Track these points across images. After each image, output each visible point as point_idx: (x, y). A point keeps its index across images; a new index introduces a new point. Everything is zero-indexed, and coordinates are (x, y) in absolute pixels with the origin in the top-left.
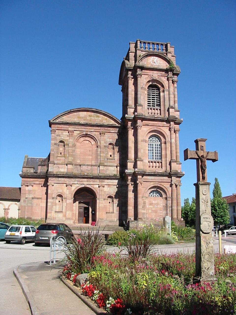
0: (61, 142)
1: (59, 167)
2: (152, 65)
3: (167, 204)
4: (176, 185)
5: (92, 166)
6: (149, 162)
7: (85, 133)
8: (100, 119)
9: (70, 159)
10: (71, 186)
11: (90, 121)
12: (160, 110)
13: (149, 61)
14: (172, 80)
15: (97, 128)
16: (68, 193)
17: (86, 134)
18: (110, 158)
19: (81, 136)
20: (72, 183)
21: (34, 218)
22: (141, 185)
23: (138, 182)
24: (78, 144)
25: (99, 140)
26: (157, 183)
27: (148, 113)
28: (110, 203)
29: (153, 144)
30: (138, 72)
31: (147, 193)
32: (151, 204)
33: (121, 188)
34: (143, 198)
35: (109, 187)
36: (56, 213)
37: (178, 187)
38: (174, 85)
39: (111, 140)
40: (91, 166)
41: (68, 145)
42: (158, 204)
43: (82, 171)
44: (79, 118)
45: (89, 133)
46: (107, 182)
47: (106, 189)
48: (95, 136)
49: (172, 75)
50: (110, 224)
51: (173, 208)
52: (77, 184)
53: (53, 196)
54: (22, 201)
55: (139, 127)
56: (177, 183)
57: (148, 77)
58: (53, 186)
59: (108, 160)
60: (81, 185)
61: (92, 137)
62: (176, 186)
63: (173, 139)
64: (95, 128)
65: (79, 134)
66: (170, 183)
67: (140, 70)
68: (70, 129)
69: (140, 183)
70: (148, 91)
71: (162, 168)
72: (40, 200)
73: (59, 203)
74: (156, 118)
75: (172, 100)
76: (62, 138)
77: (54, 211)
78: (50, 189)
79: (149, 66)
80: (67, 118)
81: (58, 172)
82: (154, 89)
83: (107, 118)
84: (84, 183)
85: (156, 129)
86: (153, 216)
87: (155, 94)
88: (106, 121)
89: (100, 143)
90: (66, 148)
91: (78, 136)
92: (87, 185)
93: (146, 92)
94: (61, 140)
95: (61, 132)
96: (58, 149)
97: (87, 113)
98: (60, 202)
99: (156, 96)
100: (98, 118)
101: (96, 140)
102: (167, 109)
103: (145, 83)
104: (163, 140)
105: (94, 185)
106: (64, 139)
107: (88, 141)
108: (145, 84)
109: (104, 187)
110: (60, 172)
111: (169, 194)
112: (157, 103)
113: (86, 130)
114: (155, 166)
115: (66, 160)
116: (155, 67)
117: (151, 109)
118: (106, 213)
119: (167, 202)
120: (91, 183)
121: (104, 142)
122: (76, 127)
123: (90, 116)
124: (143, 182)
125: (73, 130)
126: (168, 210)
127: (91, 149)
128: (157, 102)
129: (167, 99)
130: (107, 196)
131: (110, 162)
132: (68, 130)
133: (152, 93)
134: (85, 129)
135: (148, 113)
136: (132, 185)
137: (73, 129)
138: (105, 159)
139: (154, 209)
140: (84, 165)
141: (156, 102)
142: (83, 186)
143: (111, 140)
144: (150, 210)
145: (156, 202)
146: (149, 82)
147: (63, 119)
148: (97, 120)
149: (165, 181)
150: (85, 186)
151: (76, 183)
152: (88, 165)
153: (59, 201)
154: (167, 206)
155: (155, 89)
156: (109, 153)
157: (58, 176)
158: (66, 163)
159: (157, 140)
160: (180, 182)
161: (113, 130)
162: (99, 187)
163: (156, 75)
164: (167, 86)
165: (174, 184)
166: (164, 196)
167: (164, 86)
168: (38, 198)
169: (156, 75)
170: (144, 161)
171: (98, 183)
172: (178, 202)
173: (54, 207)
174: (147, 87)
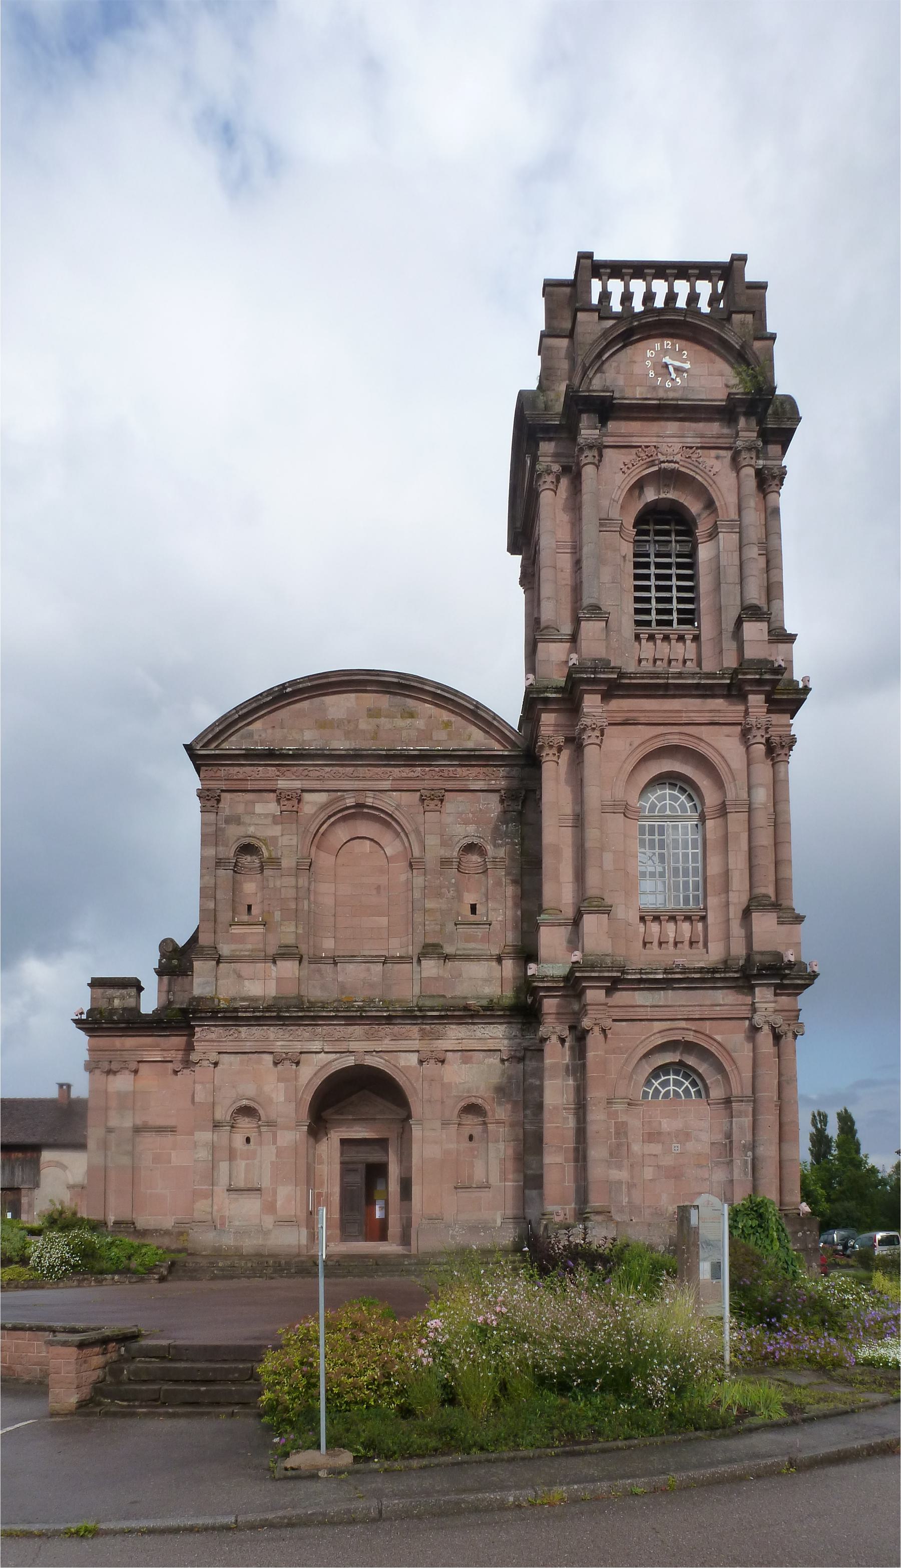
0: (248, 849)
1: (243, 974)
2: (655, 388)
3: (729, 1136)
4: (773, 1029)
6: (642, 919)
7: (350, 802)
9: (288, 933)
10: (298, 1063)
11: (375, 736)
12: (696, 638)
13: (637, 369)
14: (768, 740)
15: (406, 772)
16: (282, 1099)
17: (359, 806)
18: (472, 918)
19: (332, 819)
20: (298, 1046)
21: (143, 1222)
22: (606, 1036)
23: (586, 1023)
24: (325, 860)
25: (417, 831)
26: (683, 1024)
27: (640, 661)
28: (471, 1138)
29: (662, 828)
30: (583, 432)
31: (631, 1078)
33: (521, 1066)
34: (615, 1107)
35: (465, 1062)
36: (234, 1195)
37: (788, 1039)
38: (773, 765)
40: (384, 963)
41: (275, 862)
42: (685, 1135)
43: (342, 988)
44: (324, 724)
45: (369, 801)
46: (455, 1035)
48: (397, 815)
49: (755, 434)
51: (761, 1150)
52: (324, 1054)
53: (218, 1116)
54: (91, 1144)
55: (589, 733)
56: (779, 1020)
57: (635, 456)
58: (216, 1064)
59: (462, 929)
60: (338, 1055)
61: (384, 819)
62: (777, 1037)
63: (761, 785)
66: (747, 1022)
67: (595, 418)
68: (282, 784)
69: (597, 1029)
70: (635, 541)
71: (706, 945)
72: (169, 1138)
73: (247, 1147)
75: (754, 573)
76: (251, 830)
77: (226, 1188)
78: (202, 1083)
79: (637, 393)
80: (270, 731)
81: (234, 999)
82: (667, 533)
83: (453, 718)
84: (353, 1046)
85: (675, 740)
87: (669, 556)
88: (449, 734)
90: (267, 880)
91: (323, 816)
92: (366, 1057)
93: (627, 549)
94: (247, 841)
95: (247, 803)
96: (235, 888)
97: (357, 698)
98: (252, 1143)
100: (409, 721)
101: (402, 834)
103: (620, 494)
104: (711, 798)
105: (397, 1053)
106: (258, 834)
107: (368, 842)
108: (621, 501)
109: (443, 1062)
110: (243, 999)
111: (740, 1083)
113: (350, 782)
114: (671, 940)
116: (671, 395)
117: (651, 638)
118: (456, 1188)
119: (731, 1122)
120: (387, 1044)
121: (439, 841)
122: (311, 774)
123: (373, 713)
124: (614, 1020)
125: (299, 786)
126: (738, 1163)
129: (731, 573)
130: (459, 1107)
131: (469, 939)
132: (274, 791)
133: (657, 556)
134: (351, 778)
135: (640, 661)
136: (563, 1041)
137: (297, 784)
138: (443, 925)
139: (668, 1161)
140: (351, 958)
141: (675, 601)
142: (350, 1061)
143: (471, 829)
144: (651, 1169)
146: (639, 486)
147: (250, 735)
148: (404, 733)
149: (718, 1012)
150: (357, 1063)
151: (316, 1046)
152: (370, 960)
153: (248, 1140)
154: (731, 1142)
155: (673, 527)
156: (466, 894)
157: (232, 1016)
158: (272, 950)
159: (682, 806)
160: (798, 1016)
161: (481, 777)
162: (421, 1062)
164: (731, 499)
165: (766, 1029)
166: (716, 1093)
167: (717, 504)
168: (160, 1130)
169: (670, 441)
170: (620, 912)
171: (416, 1045)
172: (786, 1119)
173: (224, 1166)
174: (629, 521)
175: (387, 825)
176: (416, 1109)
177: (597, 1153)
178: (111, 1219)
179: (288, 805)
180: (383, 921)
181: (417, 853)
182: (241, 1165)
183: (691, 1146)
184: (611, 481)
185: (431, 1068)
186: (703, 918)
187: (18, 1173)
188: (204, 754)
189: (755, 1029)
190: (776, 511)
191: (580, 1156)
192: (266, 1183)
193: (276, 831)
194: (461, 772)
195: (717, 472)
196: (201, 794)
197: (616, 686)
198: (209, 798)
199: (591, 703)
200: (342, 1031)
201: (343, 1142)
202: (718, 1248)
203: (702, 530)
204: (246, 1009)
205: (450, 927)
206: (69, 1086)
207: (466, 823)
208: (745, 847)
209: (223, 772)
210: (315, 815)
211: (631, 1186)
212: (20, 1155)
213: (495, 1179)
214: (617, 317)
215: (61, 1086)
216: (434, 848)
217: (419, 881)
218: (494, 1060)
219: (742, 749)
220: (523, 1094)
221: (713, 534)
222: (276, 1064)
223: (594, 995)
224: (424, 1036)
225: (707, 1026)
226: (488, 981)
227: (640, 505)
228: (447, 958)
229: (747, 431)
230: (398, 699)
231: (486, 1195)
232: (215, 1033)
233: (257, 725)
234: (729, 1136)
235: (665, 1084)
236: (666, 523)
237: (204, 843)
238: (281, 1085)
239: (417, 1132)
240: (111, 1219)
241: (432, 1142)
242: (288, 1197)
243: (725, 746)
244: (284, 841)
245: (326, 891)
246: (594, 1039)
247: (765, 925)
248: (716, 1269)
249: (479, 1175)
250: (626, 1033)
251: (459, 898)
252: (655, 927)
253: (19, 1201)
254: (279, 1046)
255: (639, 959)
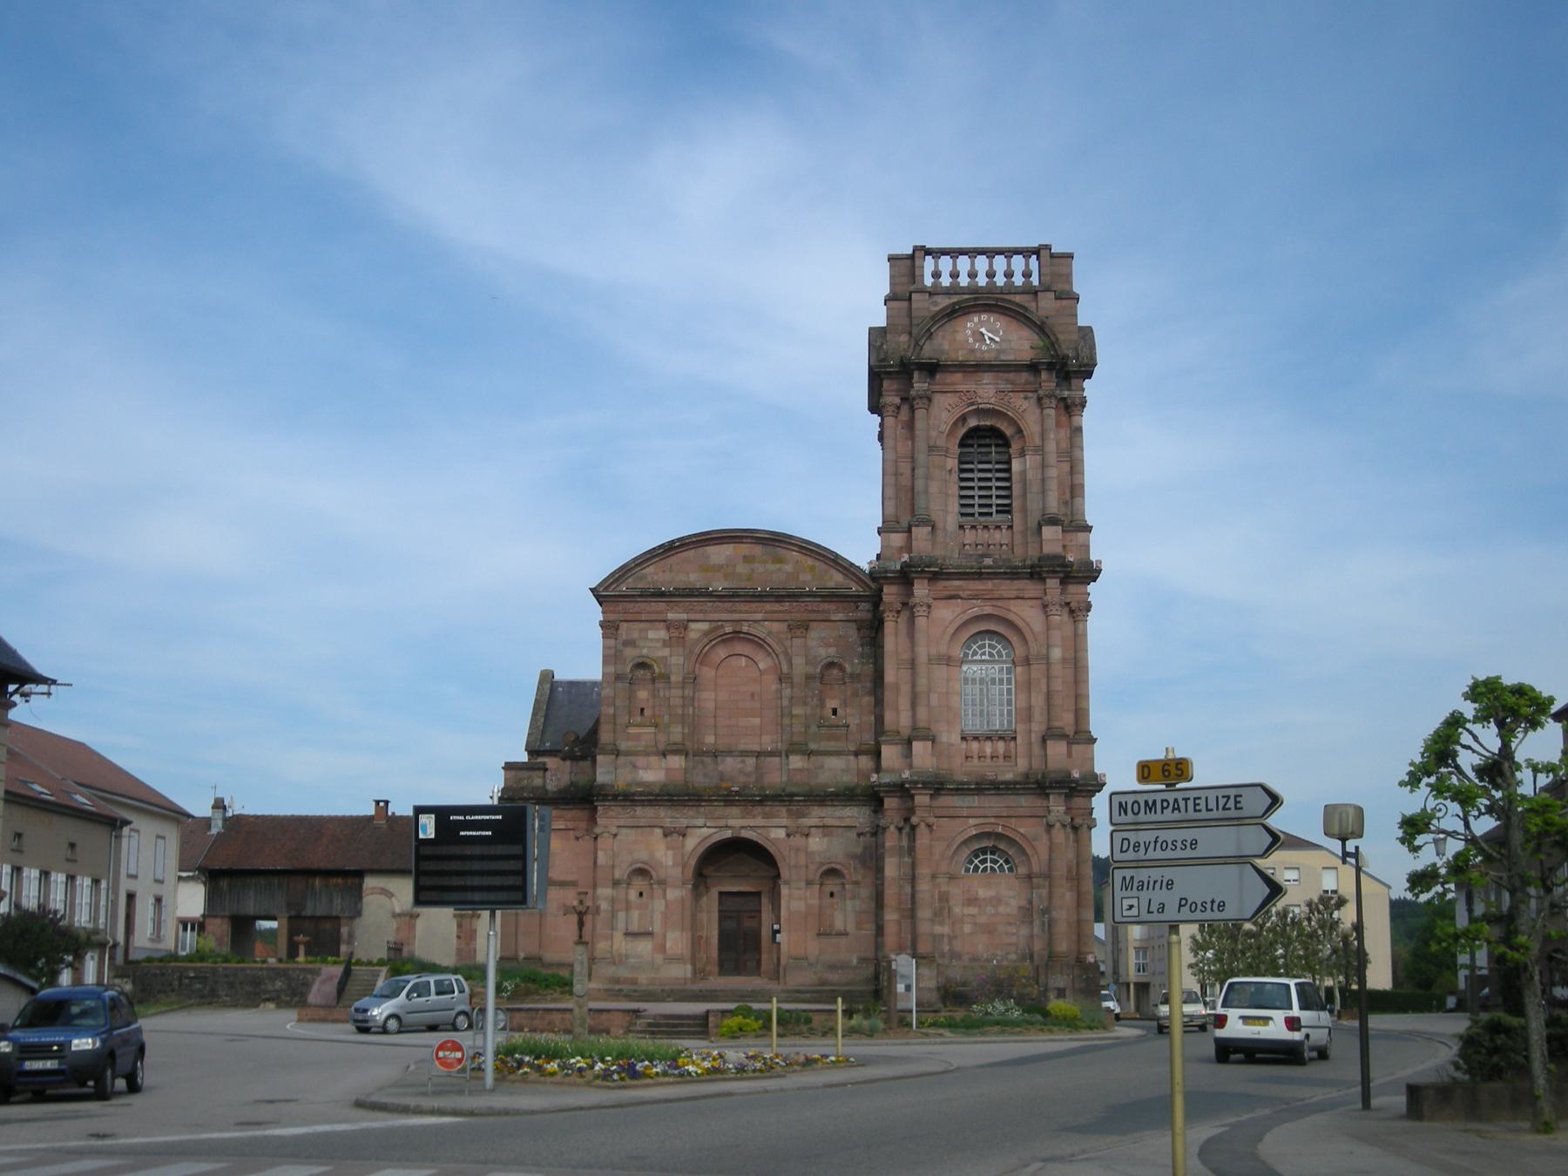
0: (642, 665)
2: (973, 351)
3: (1030, 902)
5: (759, 754)
6: (964, 738)
7: (728, 629)
8: (789, 568)
9: (677, 733)
11: (749, 578)
12: (1010, 527)
13: (959, 337)
15: (777, 607)
16: (670, 863)
20: (684, 822)
23: (914, 820)
24: (707, 673)
25: (786, 653)
28: (832, 895)
32: (972, 901)
39: (832, 651)
41: (666, 677)
42: (997, 901)
43: (722, 777)
44: (706, 568)
45: (745, 629)
46: (816, 815)
47: (816, 843)
48: (769, 640)
50: (834, 977)
52: (704, 830)
53: (617, 876)
64: (768, 607)
65: (706, 634)
68: (670, 616)
74: (545, 847)
76: (645, 651)
82: (989, 446)
83: (817, 564)
84: (731, 822)
86: (981, 945)
89: (791, 664)
91: (705, 641)
93: (952, 463)
96: (631, 696)
99: (998, 471)
102: (1032, 524)
103: (945, 428)
105: (772, 830)
112: (1000, 502)
113: (725, 615)
115: (662, 738)
116: (987, 356)
120: (759, 821)
123: (748, 559)
127: (756, 688)
128: (998, 497)
129: (1035, 487)
137: (684, 616)
139: (983, 919)
140: (730, 753)
142: (728, 834)
143: (832, 651)
145: (991, 893)
149: (1021, 811)
153: (641, 894)
155: (993, 441)
157: (628, 798)
158: (661, 747)
159: (999, 653)
162: (788, 835)
163: (987, 390)
169: (987, 390)
171: (785, 822)
173: (621, 915)
175: (761, 646)
176: (784, 873)
177: (924, 913)
178: (522, 955)
179: (675, 633)
180: (757, 721)
181: (785, 669)
182: (635, 914)
183: (1002, 909)
184: (943, 414)
185: (797, 840)
186: (1014, 739)
187: (337, 901)
188: (601, 594)
189: (1050, 827)
190: (1079, 429)
191: (911, 913)
192: (657, 927)
193: (666, 652)
194: (826, 606)
195: (1025, 410)
196: (603, 625)
197: (937, 575)
198: (608, 627)
199: (921, 590)
200: (720, 811)
201: (721, 894)
202: (909, 977)
203: (1015, 448)
204: (641, 794)
205: (814, 728)
206: (387, 802)
207: (829, 646)
208: (1044, 688)
209: (621, 606)
210: (699, 640)
211: (951, 938)
212: (340, 881)
213: (851, 928)
214: (947, 292)
215: (377, 802)
216: (800, 667)
217: (787, 692)
218: (852, 834)
219: (1042, 617)
220: (872, 860)
221: (1022, 454)
222: (665, 835)
223: (922, 799)
224: (790, 814)
225: (1013, 823)
226: (846, 771)
227: (964, 430)
228: (810, 753)
229: (1048, 381)
230: (770, 549)
231: (843, 940)
232: (616, 810)
233: (651, 569)
234: (1030, 902)
235: (984, 861)
236: (986, 440)
237: (605, 662)
238: (670, 853)
239: (784, 890)
240: (522, 955)
241: (796, 898)
242: (677, 941)
243: (1027, 614)
244: (674, 660)
245: (708, 698)
246: (922, 830)
247: (1057, 749)
248: (908, 988)
249: (839, 925)
250: (948, 829)
251: (822, 705)
252: (975, 745)
253: (339, 931)
254: (668, 823)
255: (961, 770)
